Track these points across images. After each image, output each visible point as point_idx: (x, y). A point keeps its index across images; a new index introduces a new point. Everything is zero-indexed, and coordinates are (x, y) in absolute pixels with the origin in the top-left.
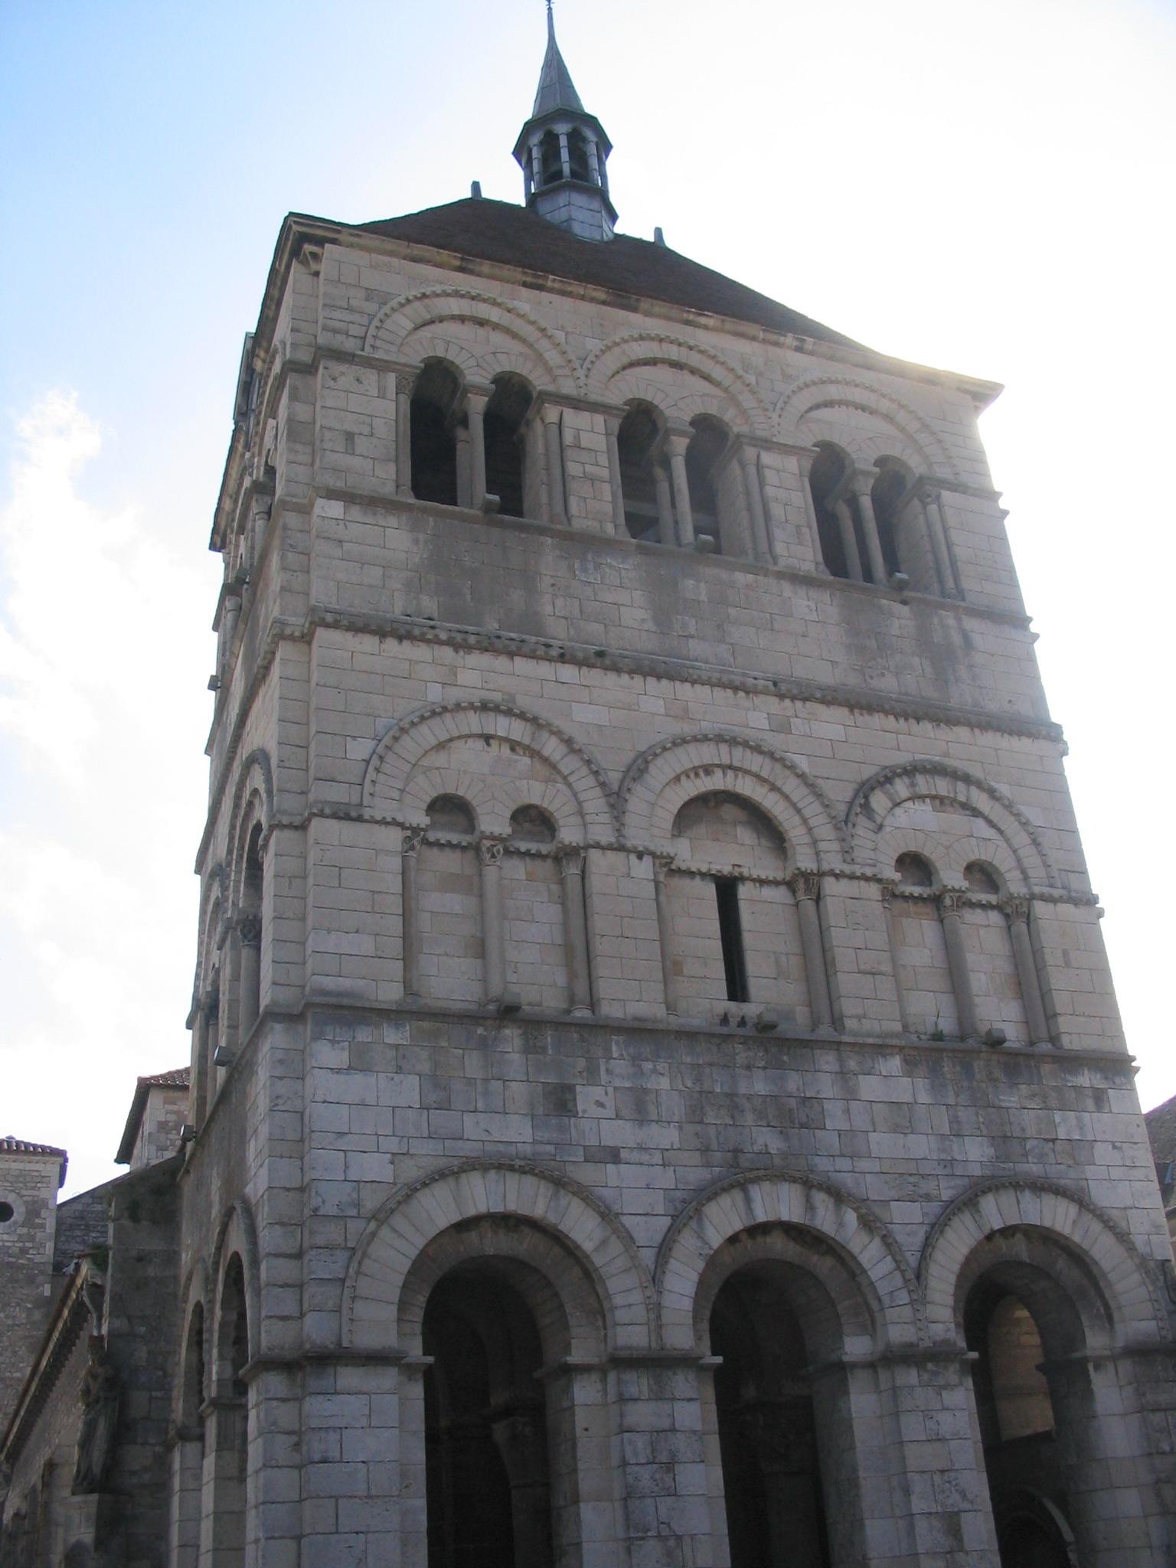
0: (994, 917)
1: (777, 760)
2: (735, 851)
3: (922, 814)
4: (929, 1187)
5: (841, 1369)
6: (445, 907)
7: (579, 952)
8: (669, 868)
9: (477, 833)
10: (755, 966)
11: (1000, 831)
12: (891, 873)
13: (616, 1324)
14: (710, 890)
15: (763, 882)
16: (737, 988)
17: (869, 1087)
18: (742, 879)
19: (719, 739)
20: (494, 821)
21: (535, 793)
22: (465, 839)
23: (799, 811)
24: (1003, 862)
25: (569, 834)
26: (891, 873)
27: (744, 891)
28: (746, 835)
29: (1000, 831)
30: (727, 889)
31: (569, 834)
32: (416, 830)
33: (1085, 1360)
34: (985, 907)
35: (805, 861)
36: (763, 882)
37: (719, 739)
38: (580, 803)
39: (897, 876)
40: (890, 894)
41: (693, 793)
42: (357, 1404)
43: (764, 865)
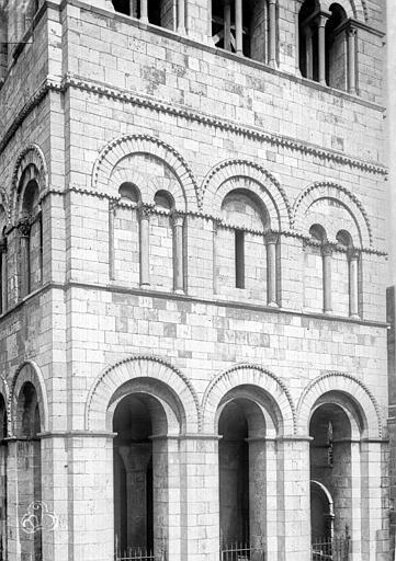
0: (344, 256)
1: (170, 150)
2: (246, 218)
3: (324, 207)
4: (304, 373)
5: (165, 438)
6: (125, 235)
7: (180, 261)
8: (218, 224)
9: (350, 246)
10: (248, 273)
11: (354, 217)
12: (307, 234)
13: (384, 442)
14: (232, 236)
15: (254, 233)
16: (240, 283)
17: (288, 330)
18: (247, 231)
19: (166, 147)
20: (148, 198)
21: (165, 185)
22: (134, 204)
23: (274, 201)
24: (353, 232)
25: (179, 206)
26: (307, 234)
27: (248, 237)
28: (249, 209)
29: (354, 217)
30: (240, 234)
31: (179, 206)
32: (116, 200)
33: (351, 442)
34: (341, 251)
35: (274, 226)
36: (254, 233)
37: (166, 147)
38: (184, 191)
39: (310, 236)
40: (115, 204)
41: (236, 187)
42: (91, 452)
43: (258, 227)
